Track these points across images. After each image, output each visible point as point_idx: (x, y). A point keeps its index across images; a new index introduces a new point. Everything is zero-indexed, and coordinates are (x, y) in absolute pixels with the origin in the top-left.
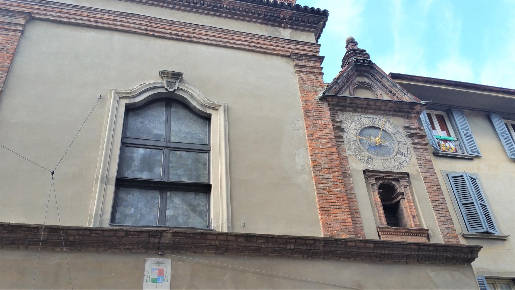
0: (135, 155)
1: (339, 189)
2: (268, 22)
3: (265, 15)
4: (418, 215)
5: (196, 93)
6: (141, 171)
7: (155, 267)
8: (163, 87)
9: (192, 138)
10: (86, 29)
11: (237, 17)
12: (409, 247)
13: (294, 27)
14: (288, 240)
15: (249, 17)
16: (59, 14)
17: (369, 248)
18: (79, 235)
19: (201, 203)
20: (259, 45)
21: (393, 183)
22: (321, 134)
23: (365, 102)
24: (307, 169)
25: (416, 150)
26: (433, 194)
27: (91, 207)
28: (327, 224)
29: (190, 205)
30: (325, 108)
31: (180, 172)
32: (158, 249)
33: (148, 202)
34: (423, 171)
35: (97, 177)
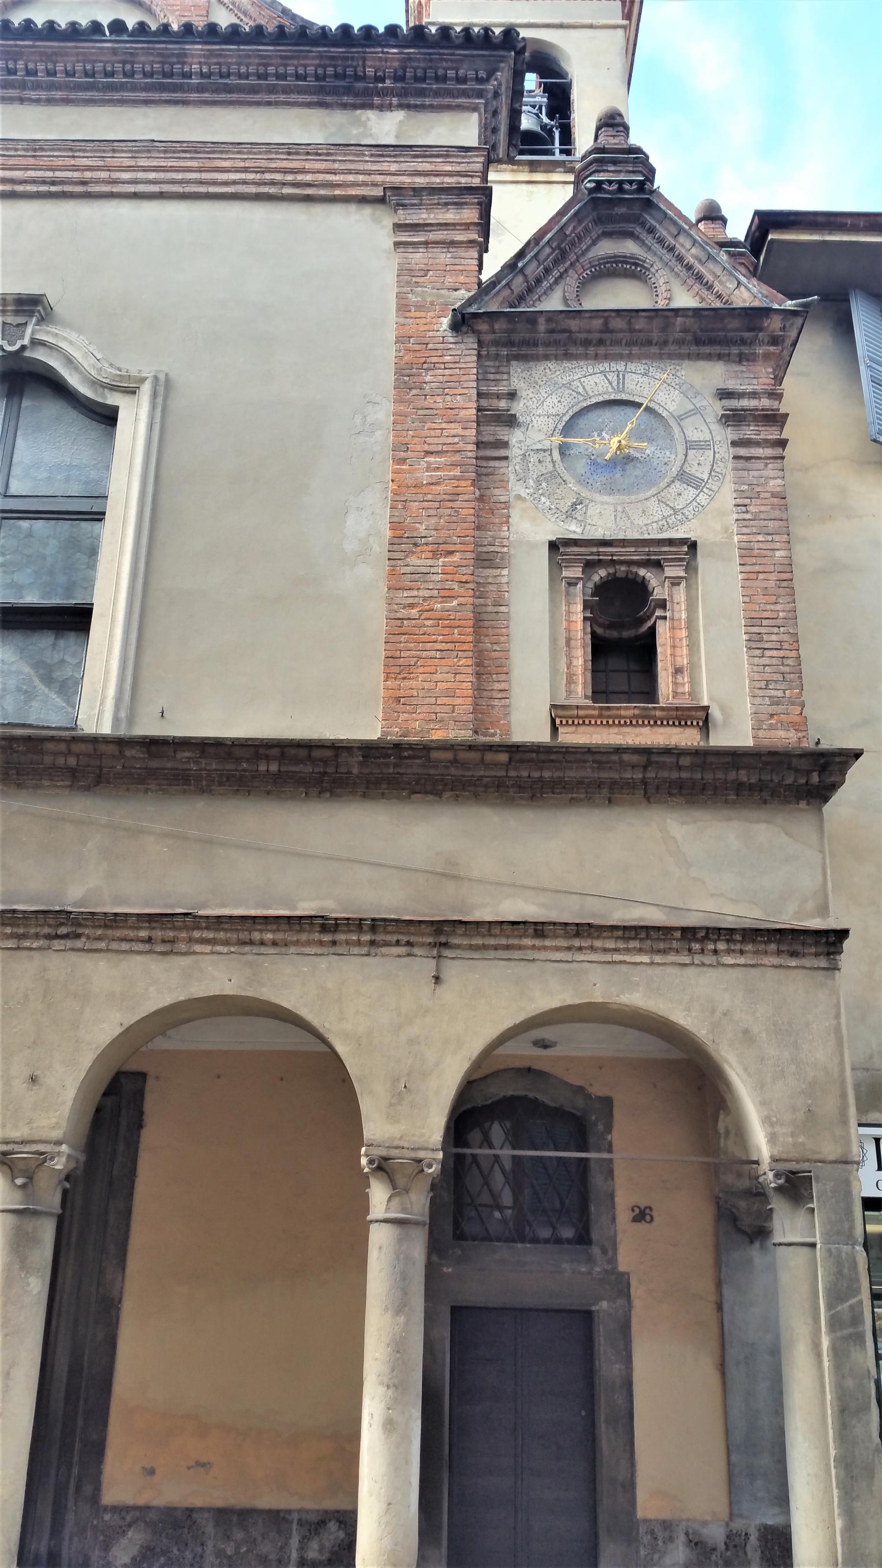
1: (455, 603)
2: (329, 99)
4: (694, 666)
9: (67, 479)
11: (235, 96)
12: (615, 758)
14: (262, 751)
17: (496, 765)
19: (68, 658)
20: (290, 178)
21: (642, 572)
22: (436, 440)
23: (597, 323)
24: (376, 548)
25: (741, 464)
26: (761, 599)
28: (396, 701)
29: (38, 665)
30: (464, 354)
34: (745, 530)
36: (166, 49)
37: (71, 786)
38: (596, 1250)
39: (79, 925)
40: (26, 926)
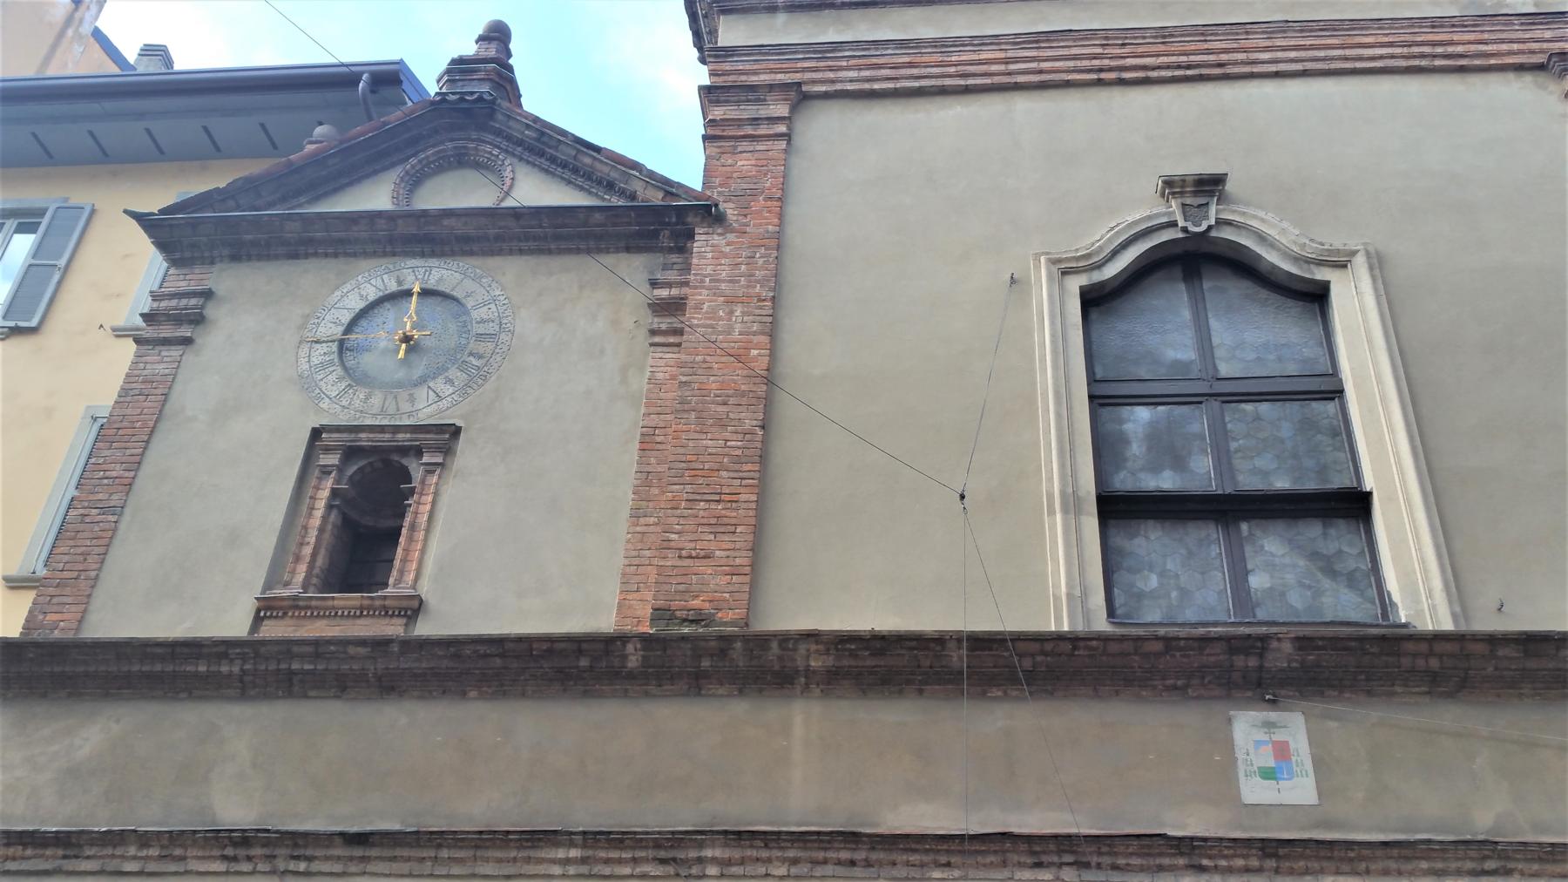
0: (1128, 427)
5: (1273, 226)
6: (1155, 469)
7: (1261, 735)
8: (1173, 224)
9: (1280, 359)
10: (939, 100)
18: (1046, 654)
19: (1346, 549)
20: (1439, 50)
27: (1054, 583)
29: (1314, 556)
31: (1265, 462)
32: (1259, 685)
33: (1190, 554)
35: (1050, 496)
39: (1508, 858)
40: (1444, 860)
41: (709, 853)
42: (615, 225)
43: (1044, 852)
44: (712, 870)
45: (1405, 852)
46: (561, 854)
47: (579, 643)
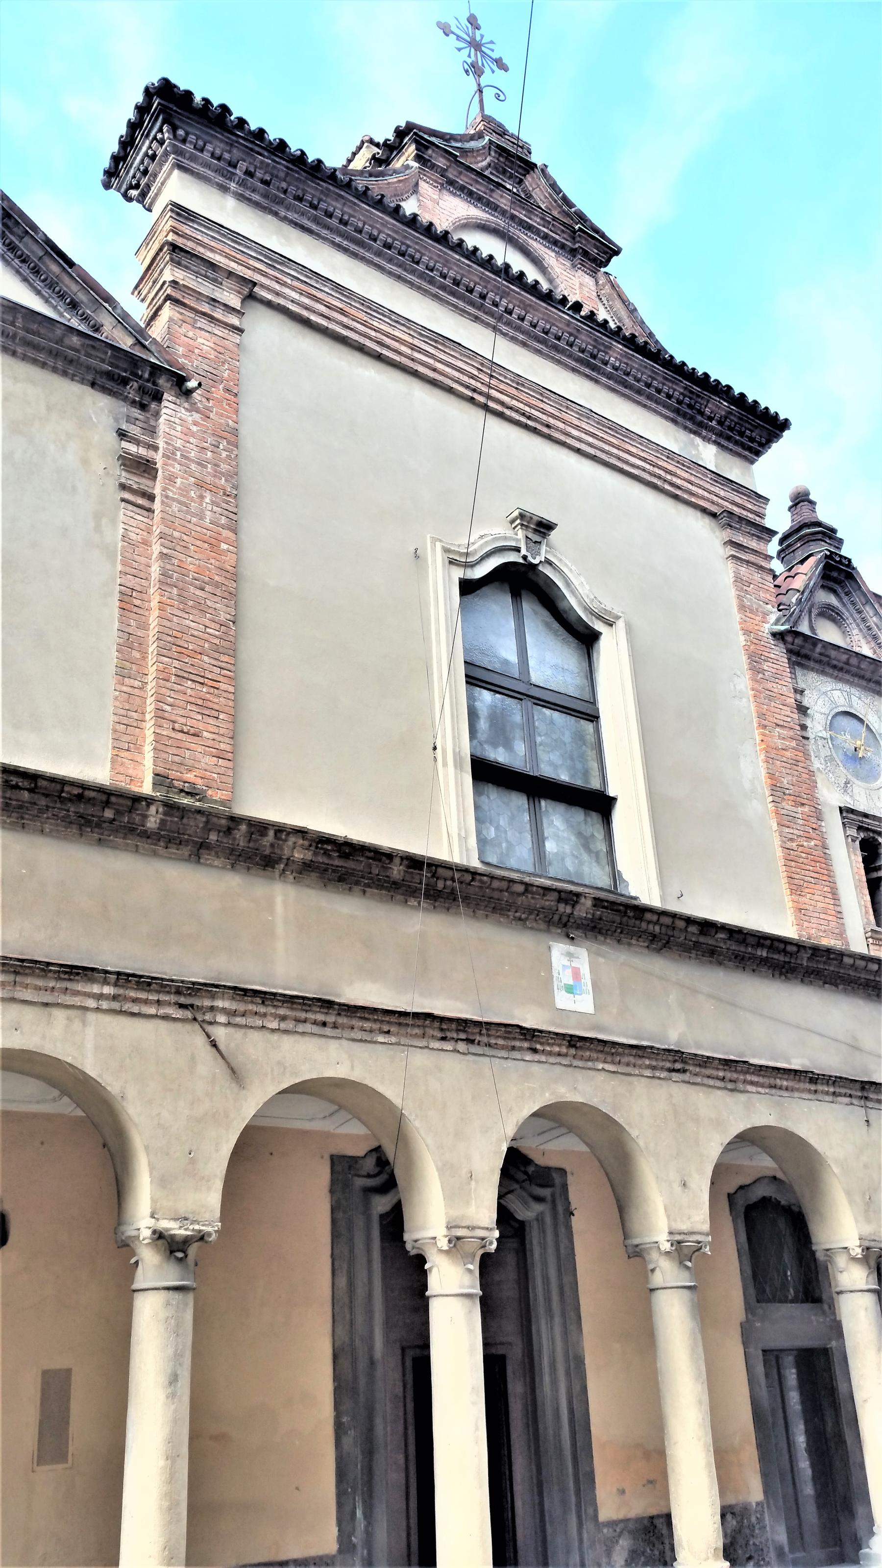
1: (813, 843)
2: (679, 419)
3: (680, 402)
6: (495, 745)
7: (565, 961)
13: (723, 442)
15: (649, 397)
16: (307, 301)
20: (669, 477)
23: (844, 657)
29: (579, 835)
31: (555, 757)
36: (601, 338)
37: (648, 947)
38: (826, 1307)
39: (685, 1063)
40: (656, 1060)
41: (220, 1003)
42: (88, 355)
43: (448, 1030)
44: (222, 1019)
45: (640, 1053)
46: (96, 989)
47: (107, 796)
